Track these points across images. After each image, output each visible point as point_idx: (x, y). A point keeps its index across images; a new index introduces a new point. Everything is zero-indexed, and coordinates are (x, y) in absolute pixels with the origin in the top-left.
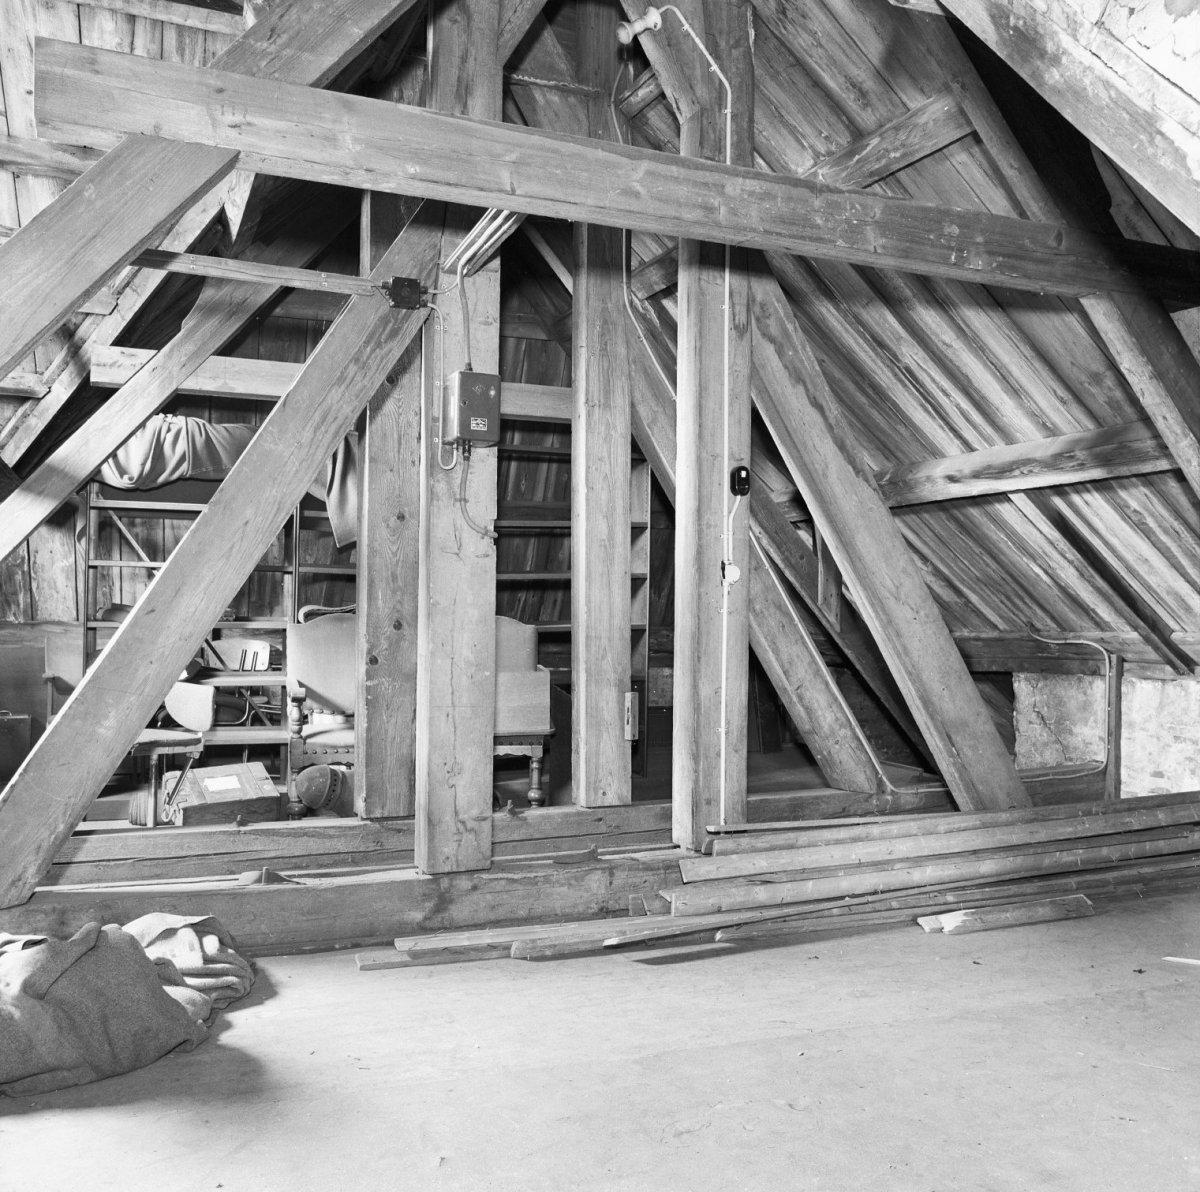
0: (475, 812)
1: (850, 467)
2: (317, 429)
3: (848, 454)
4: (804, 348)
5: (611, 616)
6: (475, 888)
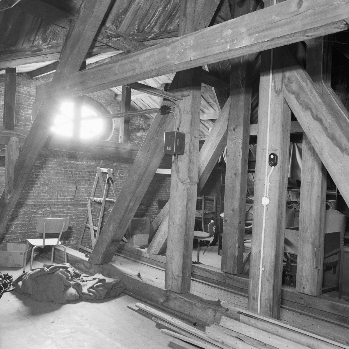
0: (177, 274)
1: (338, 148)
2: (147, 153)
3: (337, 142)
4: (311, 92)
5: (311, 215)
6: (175, 298)
